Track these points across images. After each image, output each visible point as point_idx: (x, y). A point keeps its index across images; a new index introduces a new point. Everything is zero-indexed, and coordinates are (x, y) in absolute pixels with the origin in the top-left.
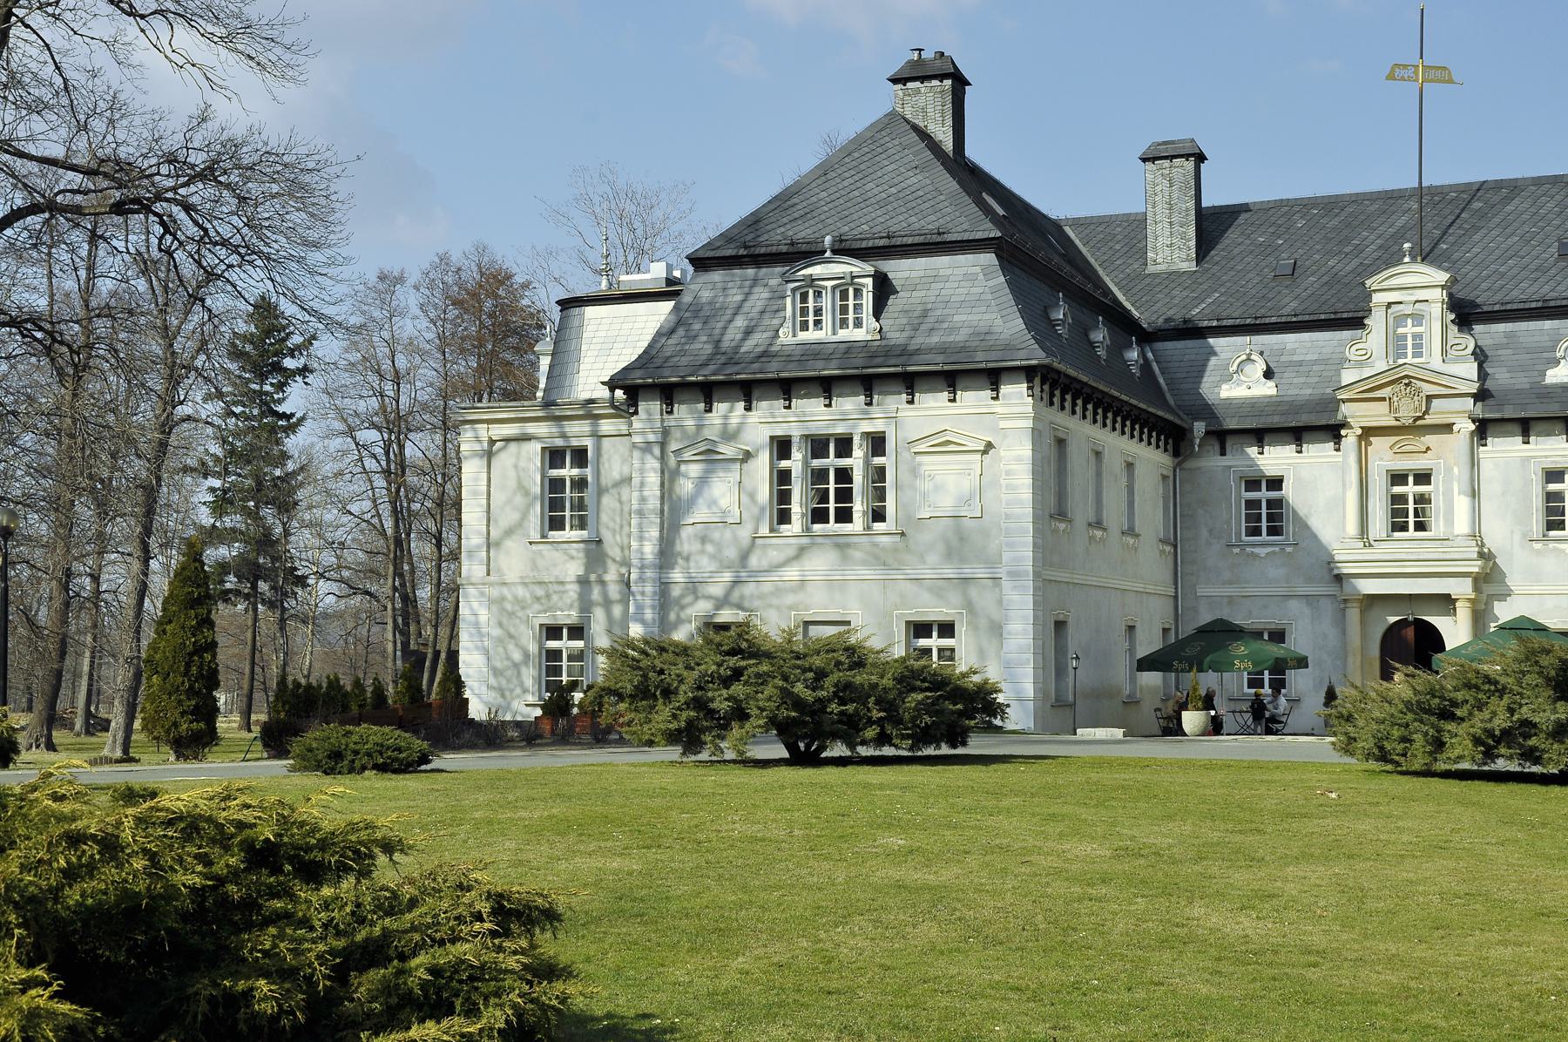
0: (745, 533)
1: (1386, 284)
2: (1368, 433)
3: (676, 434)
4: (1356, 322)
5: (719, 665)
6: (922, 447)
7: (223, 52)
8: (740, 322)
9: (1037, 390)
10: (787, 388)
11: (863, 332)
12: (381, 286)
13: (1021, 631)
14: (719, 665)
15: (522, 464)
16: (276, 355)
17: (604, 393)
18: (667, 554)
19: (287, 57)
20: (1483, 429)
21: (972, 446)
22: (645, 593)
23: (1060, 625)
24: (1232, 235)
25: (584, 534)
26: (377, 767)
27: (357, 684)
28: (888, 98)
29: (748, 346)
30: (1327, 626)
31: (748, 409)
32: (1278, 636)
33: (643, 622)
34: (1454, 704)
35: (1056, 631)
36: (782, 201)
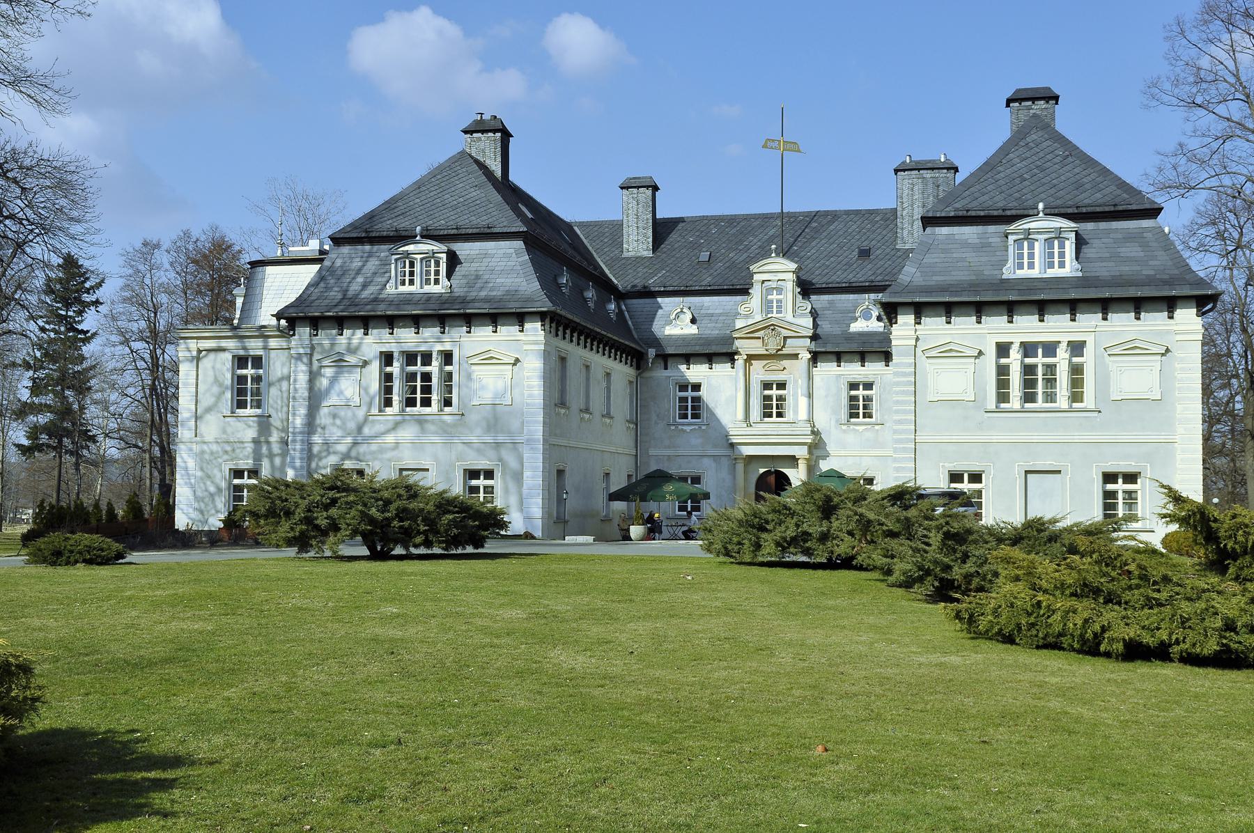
0: (361, 413)
1: (761, 269)
2: (751, 358)
3: (318, 349)
4: (744, 291)
5: (322, 496)
6: (475, 360)
7: (11, 92)
8: (360, 279)
9: (547, 327)
10: (391, 322)
11: (439, 288)
12: (144, 250)
13: (534, 476)
14: (322, 496)
15: (218, 366)
16: (77, 291)
17: (274, 322)
18: (311, 425)
19: (56, 97)
20: (815, 357)
21: (969, 353)
22: (296, 449)
23: (560, 473)
24: (674, 236)
25: (259, 411)
26: (85, 561)
27: (97, 506)
28: (461, 142)
29: (366, 294)
30: (725, 474)
31: (366, 334)
32: (696, 480)
33: (294, 468)
34: (767, 522)
35: (557, 477)
36: (390, 205)
